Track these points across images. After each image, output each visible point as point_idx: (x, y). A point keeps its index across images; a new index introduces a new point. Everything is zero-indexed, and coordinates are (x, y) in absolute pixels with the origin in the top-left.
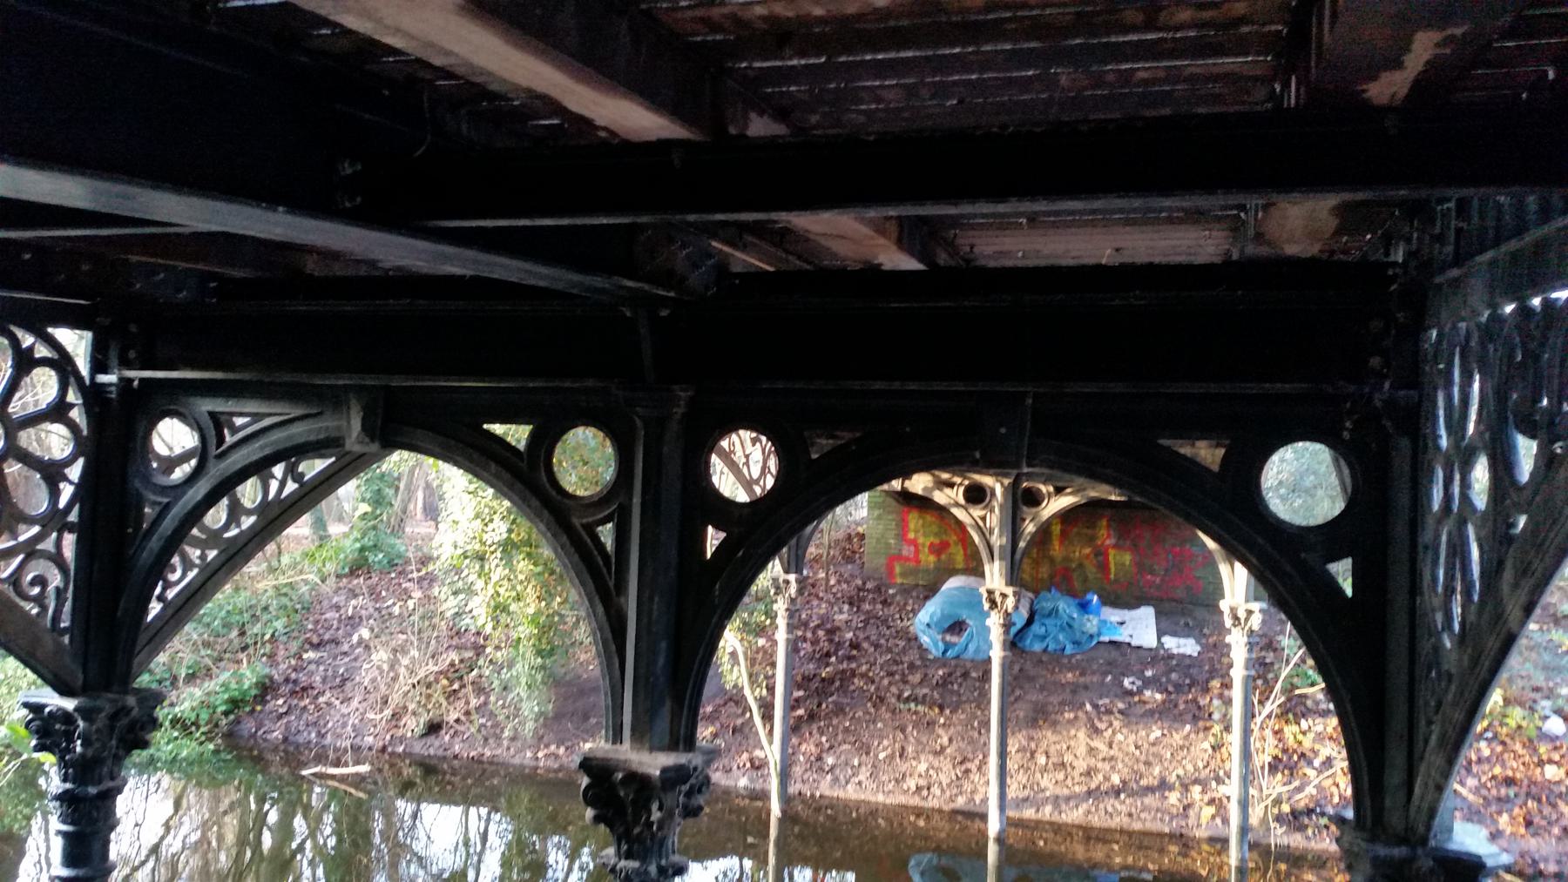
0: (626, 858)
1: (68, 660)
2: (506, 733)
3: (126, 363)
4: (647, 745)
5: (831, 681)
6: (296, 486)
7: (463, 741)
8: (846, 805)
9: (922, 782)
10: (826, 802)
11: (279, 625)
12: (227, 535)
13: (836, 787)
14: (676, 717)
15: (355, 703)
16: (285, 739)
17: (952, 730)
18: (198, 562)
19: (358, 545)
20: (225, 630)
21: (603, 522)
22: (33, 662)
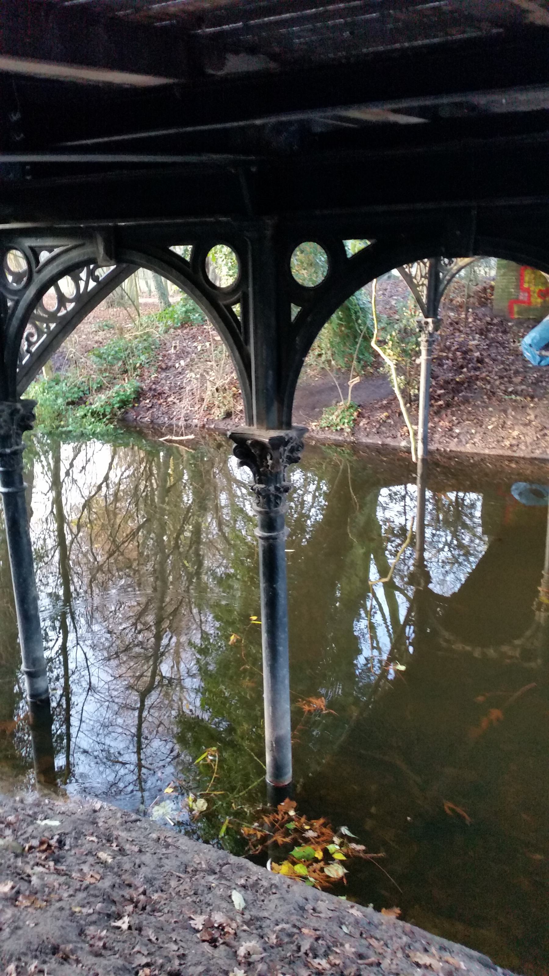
4: (265, 426)
5: (461, 383)
6: (95, 284)
9: (514, 442)
12: (60, 314)
14: (280, 411)
16: (152, 422)
17: (538, 410)
18: (45, 330)
19: (184, 309)
21: (235, 303)
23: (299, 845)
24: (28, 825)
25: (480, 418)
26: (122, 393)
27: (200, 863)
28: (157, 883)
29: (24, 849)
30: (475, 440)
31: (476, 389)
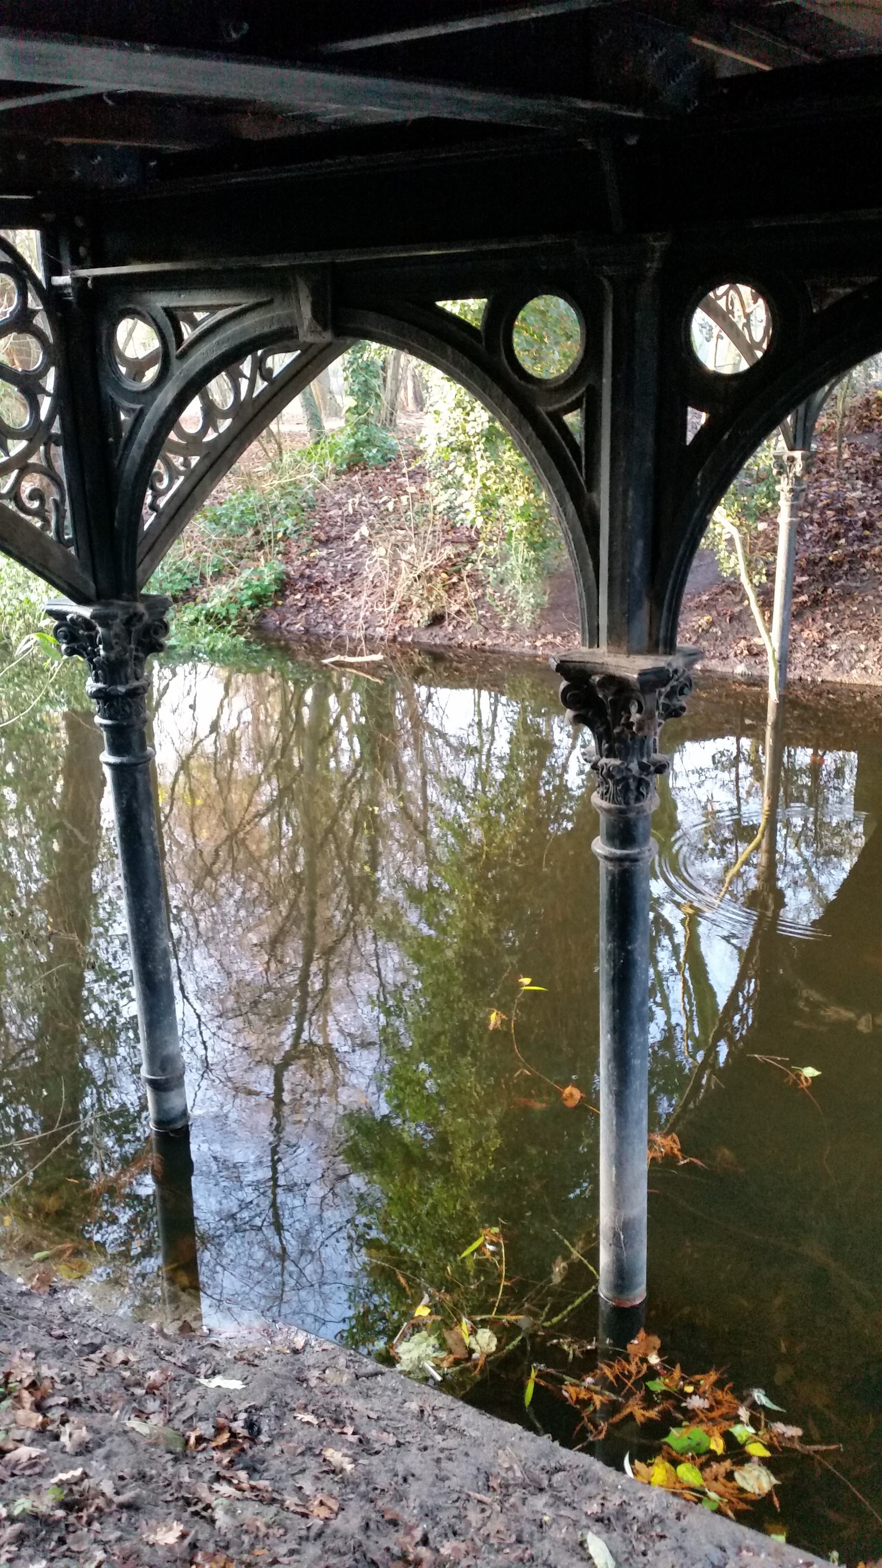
0: (607, 757)
1: (77, 569)
2: (506, 624)
3: (78, 262)
4: (625, 648)
5: (839, 564)
7: (465, 631)
8: (851, 690)
10: (829, 686)
11: (289, 523)
12: (206, 439)
13: (839, 673)
15: (364, 597)
16: (307, 631)
18: (182, 468)
19: (352, 441)
20: (242, 530)
22: (46, 572)
23: (678, 1424)
24: (187, 1390)
25: (873, 625)
26: (255, 582)
27: (510, 1469)
28: (445, 1517)
29: (187, 1442)
30: (866, 662)
31: (864, 574)
